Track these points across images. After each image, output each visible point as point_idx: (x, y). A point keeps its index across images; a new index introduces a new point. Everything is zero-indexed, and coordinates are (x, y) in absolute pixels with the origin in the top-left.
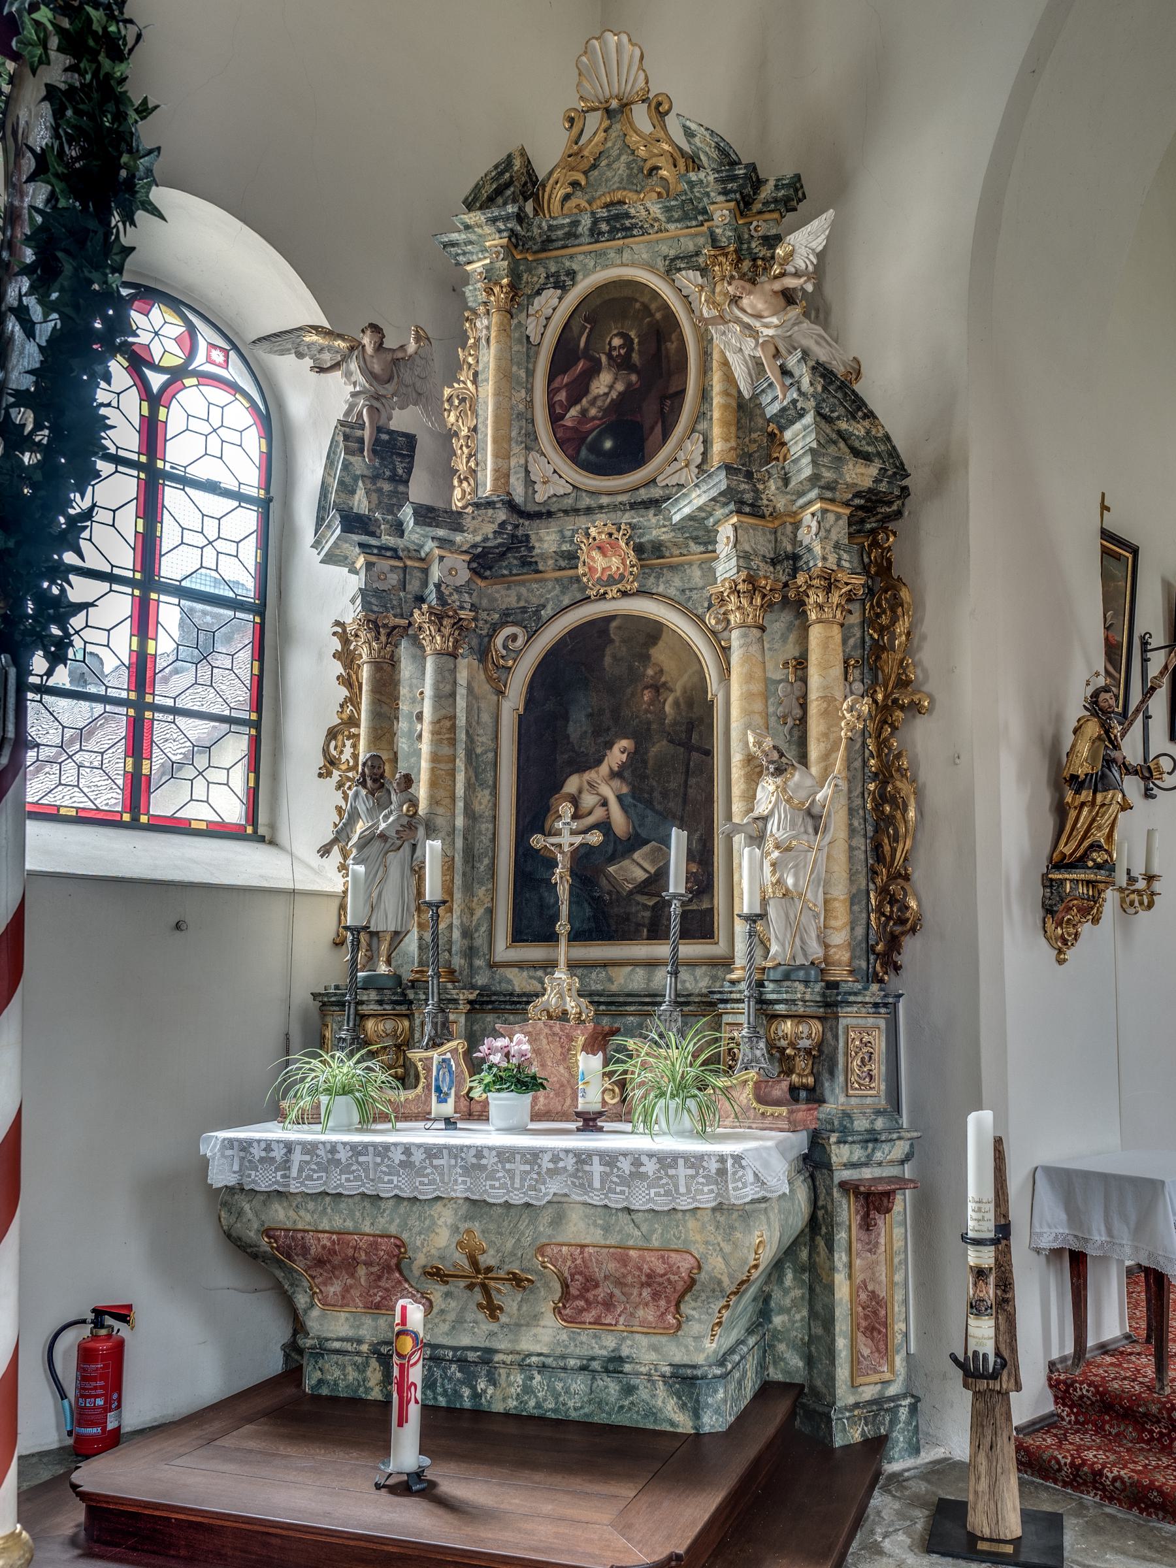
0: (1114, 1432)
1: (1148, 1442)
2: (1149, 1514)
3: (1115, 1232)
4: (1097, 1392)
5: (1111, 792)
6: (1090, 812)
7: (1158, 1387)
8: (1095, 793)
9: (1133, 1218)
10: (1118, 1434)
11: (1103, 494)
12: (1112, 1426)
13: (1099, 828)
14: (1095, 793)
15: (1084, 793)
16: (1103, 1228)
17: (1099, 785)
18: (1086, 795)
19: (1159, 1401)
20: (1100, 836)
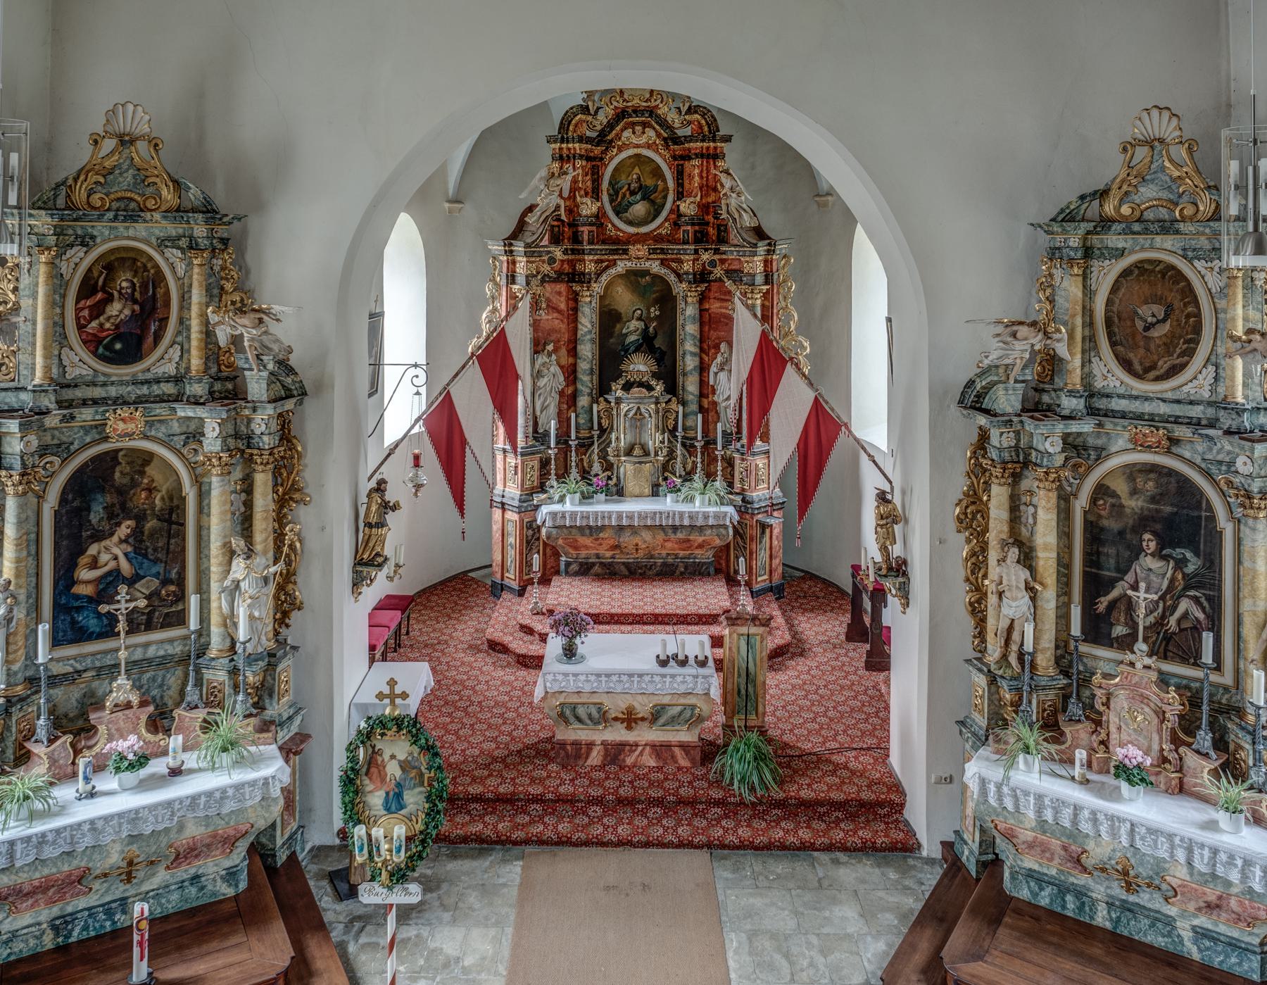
20: (378, 549)
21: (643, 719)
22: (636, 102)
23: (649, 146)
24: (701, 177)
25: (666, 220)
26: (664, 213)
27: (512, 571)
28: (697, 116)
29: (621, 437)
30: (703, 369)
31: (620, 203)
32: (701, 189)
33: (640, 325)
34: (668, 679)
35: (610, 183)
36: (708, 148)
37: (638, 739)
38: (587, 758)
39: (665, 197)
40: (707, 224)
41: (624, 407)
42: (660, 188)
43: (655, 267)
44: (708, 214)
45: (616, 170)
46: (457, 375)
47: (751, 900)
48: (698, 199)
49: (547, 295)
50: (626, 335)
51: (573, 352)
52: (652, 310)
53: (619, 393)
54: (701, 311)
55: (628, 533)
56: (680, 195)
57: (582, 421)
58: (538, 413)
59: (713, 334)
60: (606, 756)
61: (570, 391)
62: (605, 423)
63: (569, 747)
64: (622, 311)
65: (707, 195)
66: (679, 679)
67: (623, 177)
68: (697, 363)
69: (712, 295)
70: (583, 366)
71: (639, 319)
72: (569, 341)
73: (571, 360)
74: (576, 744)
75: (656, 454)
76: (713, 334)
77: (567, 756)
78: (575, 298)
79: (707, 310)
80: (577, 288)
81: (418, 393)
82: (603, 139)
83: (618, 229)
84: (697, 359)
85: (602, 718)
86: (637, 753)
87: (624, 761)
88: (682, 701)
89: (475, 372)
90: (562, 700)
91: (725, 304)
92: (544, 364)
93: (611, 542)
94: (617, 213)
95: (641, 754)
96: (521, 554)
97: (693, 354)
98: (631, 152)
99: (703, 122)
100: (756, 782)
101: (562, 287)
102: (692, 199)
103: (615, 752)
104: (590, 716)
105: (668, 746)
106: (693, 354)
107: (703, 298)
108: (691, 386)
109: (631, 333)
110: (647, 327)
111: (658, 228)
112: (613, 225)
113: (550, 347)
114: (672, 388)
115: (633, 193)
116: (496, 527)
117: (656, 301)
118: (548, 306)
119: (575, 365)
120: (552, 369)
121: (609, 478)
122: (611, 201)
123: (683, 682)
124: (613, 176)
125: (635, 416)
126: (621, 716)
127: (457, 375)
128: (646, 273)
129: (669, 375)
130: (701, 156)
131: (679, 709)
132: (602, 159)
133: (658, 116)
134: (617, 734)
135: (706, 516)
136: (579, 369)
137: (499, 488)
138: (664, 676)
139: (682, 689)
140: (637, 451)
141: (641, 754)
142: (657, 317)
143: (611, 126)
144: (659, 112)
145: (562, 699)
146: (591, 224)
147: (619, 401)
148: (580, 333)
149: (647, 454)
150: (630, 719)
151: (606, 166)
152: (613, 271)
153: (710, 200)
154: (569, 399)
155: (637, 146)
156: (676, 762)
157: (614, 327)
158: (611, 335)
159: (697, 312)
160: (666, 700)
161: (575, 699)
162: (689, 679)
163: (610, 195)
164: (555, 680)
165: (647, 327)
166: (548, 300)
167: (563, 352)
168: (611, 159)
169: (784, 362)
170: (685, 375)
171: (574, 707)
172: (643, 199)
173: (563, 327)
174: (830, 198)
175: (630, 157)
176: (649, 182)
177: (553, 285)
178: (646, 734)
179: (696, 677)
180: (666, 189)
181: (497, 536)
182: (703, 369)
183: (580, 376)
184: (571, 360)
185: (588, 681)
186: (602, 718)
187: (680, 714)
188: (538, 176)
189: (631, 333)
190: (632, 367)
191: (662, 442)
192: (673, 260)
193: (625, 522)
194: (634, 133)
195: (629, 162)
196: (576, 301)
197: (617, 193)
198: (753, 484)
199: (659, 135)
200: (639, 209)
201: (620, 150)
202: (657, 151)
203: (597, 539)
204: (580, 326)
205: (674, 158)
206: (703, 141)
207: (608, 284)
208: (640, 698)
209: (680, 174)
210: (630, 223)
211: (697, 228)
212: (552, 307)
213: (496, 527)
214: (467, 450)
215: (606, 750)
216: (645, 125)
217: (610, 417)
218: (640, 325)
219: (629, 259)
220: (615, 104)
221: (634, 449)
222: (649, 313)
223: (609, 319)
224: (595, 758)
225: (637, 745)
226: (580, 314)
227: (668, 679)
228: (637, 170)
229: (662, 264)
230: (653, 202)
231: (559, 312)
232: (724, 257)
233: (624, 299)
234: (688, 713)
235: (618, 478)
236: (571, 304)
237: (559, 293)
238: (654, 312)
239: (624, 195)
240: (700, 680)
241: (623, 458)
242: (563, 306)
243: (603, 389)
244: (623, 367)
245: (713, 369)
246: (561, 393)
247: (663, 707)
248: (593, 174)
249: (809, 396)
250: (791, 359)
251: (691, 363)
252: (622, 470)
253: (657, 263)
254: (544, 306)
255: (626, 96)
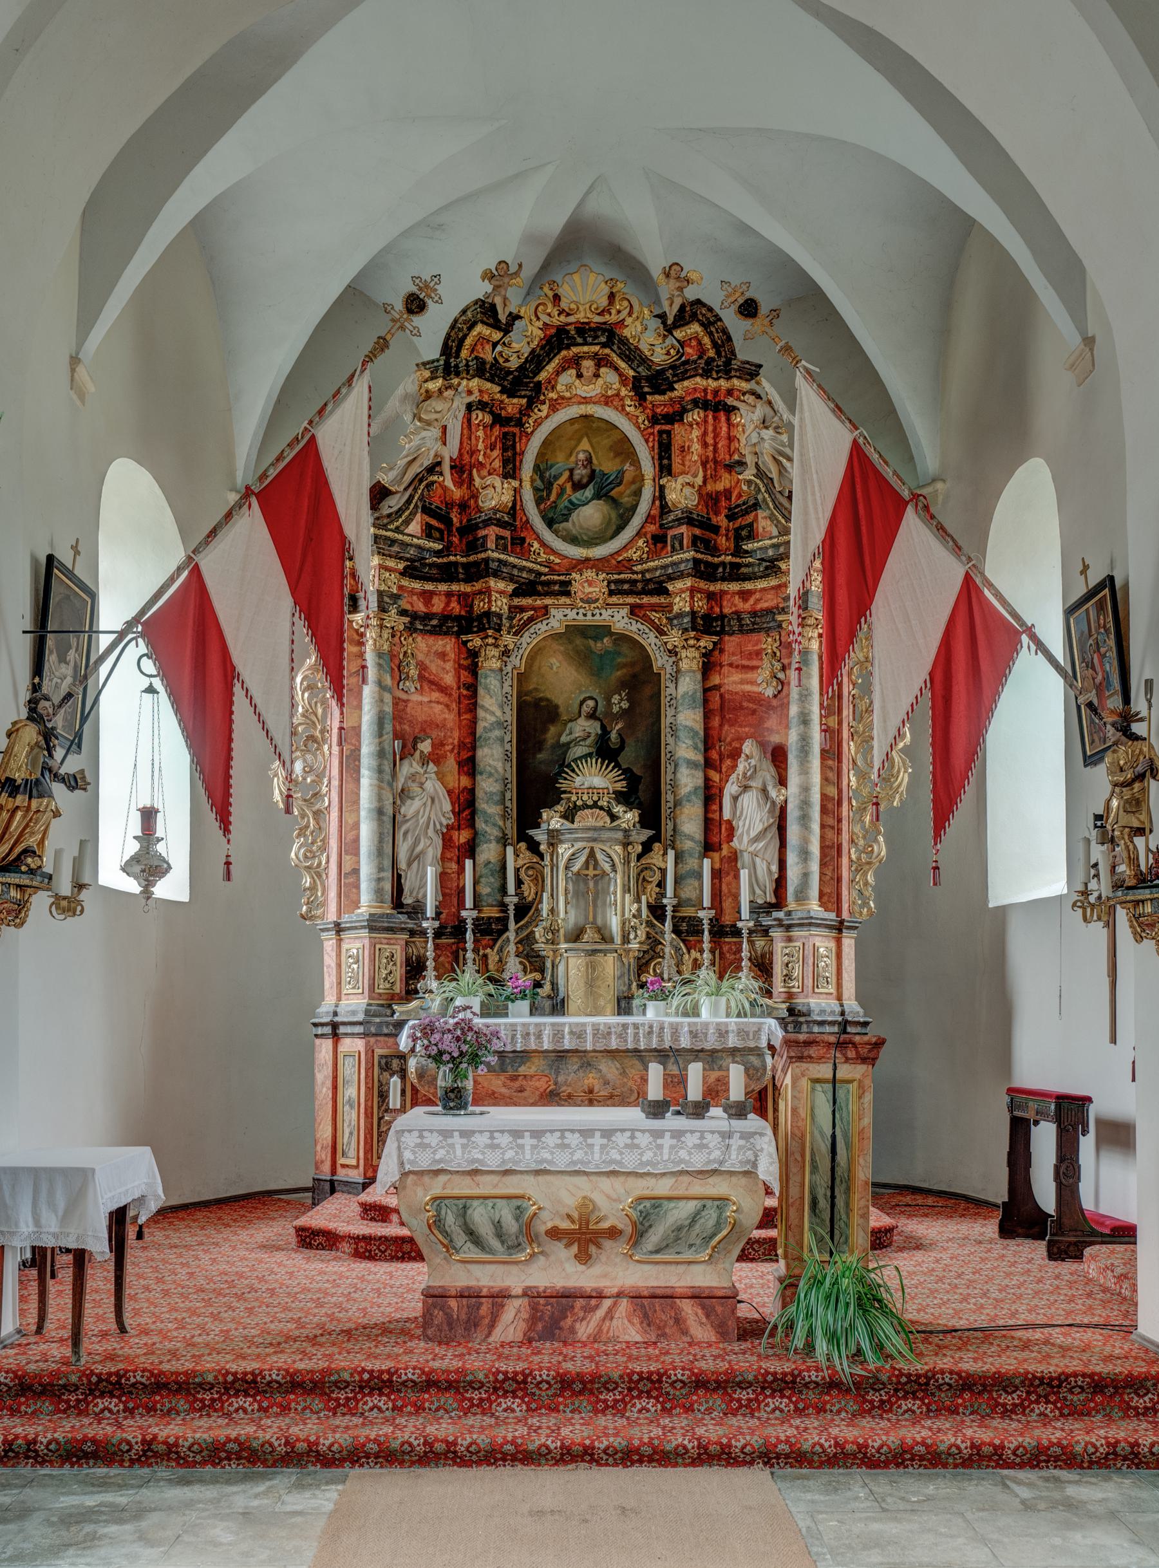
0: (29, 1411)
1: (64, 1412)
2: (81, 1466)
3: (43, 1222)
4: (16, 1376)
5: (46, 800)
6: (24, 817)
7: (73, 1360)
8: (30, 797)
9: (61, 1204)
10: (34, 1413)
11: (1114, 1040)
12: (29, 1406)
13: (32, 833)
14: (30, 797)
15: (19, 798)
16: (30, 1220)
17: (35, 792)
18: (21, 800)
19: (78, 1371)
20: (32, 841)
21: (613, 1233)
22: (581, 317)
23: (607, 401)
24: (705, 445)
25: (639, 534)
26: (636, 521)
27: (352, 1153)
28: (695, 328)
29: (560, 907)
30: (711, 796)
31: (554, 506)
32: (704, 465)
33: (594, 728)
34: (667, 1141)
35: (536, 468)
36: (716, 392)
37: (602, 1283)
38: (492, 1326)
39: (638, 493)
40: (716, 529)
41: (564, 851)
42: (628, 477)
43: (620, 620)
44: (717, 513)
45: (546, 443)
46: (213, 533)
47: (876, 1526)
48: (699, 480)
49: (420, 657)
50: (567, 746)
51: (469, 766)
52: (616, 699)
53: (556, 823)
54: (706, 691)
55: (573, 1064)
56: (665, 469)
57: (485, 890)
58: (403, 865)
59: (729, 732)
60: (533, 1320)
61: (463, 837)
62: (529, 890)
63: (453, 1303)
64: (559, 699)
65: (716, 478)
66: (691, 1140)
67: (560, 457)
68: (700, 782)
69: (726, 659)
70: (487, 786)
71: (592, 716)
72: (462, 745)
73: (465, 781)
74: (469, 1295)
75: (626, 940)
76: (729, 732)
77: (450, 1323)
78: (471, 663)
79: (717, 687)
80: (476, 641)
81: (150, 690)
82: (524, 382)
83: (553, 552)
84: (700, 775)
85: (524, 1236)
86: (600, 1313)
87: (572, 1330)
88: (699, 1188)
89: (252, 527)
90: (437, 1191)
91: (749, 676)
92: (413, 777)
93: (541, 1084)
94: (550, 523)
95: (610, 1315)
96: (369, 1115)
97: (692, 764)
98: (574, 411)
99: (706, 340)
100: (865, 1345)
101: (447, 644)
102: (688, 478)
103: (553, 1312)
104: (498, 1226)
105: (667, 1297)
106: (692, 764)
107: (708, 666)
108: (690, 822)
109: (576, 742)
110: (605, 731)
111: (625, 548)
112: (543, 544)
113: (425, 747)
114: (651, 818)
115: (578, 486)
116: (323, 1076)
117: (623, 685)
118: (421, 677)
119: (472, 791)
120: (428, 785)
121: (538, 985)
122: (539, 501)
123: (701, 1147)
124: (541, 455)
125: (587, 865)
126: (565, 1225)
127: (213, 533)
128: (604, 631)
129: (644, 794)
130: (703, 404)
131: (691, 1206)
132: (520, 424)
133: (624, 341)
134: (558, 1270)
135: (722, 1033)
136: (479, 794)
137: (330, 1000)
138: (658, 1134)
139: (698, 1161)
140: (589, 935)
141: (610, 1315)
142: (624, 713)
143: (536, 360)
144: (626, 332)
145: (438, 1187)
146: (501, 524)
147: (555, 838)
148: (481, 726)
149: (606, 938)
150: (585, 1237)
151: (529, 436)
152: (542, 628)
153: (720, 486)
154: (460, 845)
155: (586, 401)
156: (685, 1332)
157: (545, 730)
158: (540, 746)
159: (699, 687)
160: (663, 1187)
161: (464, 1187)
162: (713, 1140)
163: (536, 490)
164: (423, 1146)
165: (605, 731)
166: (422, 667)
167: (451, 764)
168: (538, 423)
169: (899, 506)
170: (677, 803)
171: (463, 1204)
172: (597, 496)
173: (450, 718)
174: (939, 486)
175: (572, 421)
176: (607, 465)
177: (431, 640)
178: (617, 1272)
179: (728, 1135)
180: (642, 478)
181: (323, 1091)
182: (711, 796)
183: (482, 805)
184: (465, 781)
185: (494, 1147)
186: (524, 1236)
187: (694, 1219)
188: (400, 391)
189: (576, 742)
190: (578, 780)
191: (637, 915)
192: (654, 608)
193: (567, 1044)
194: (579, 376)
195: (571, 429)
196: (474, 669)
197: (549, 486)
198: (809, 982)
199: (623, 379)
200: (591, 514)
201: (554, 407)
202: (622, 409)
203: (514, 1078)
204: (481, 713)
205: (654, 420)
206: (706, 374)
207: (533, 653)
208: (605, 1184)
209: (664, 451)
210: (574, 540)
211: (697, 532)
212: (427, 681)
213: (323, 1076)
214: (237, 689)
215: (534, 1308)
216: (601, 362)
217: (539, 880)
218: (594, 728)
219: (572, 606)
220: (545, 318)
221: (590, 936)
222: (609, 704)
223: (535, 717)
224: (511, 1324)
225: (601, 1296)
226: (481, 691)
227: (667, 1141)
228: (585, 445)
229: (632, 613)
230: (615, 502)
231: (443, 689)
232: (748, 586)
233: (564, 681)
234: (710, 1218)
235: (554, 985)
236: (465, 676)
237: (443, 656)
238: (619, 702)
239: (562, 489)
240: (736, 1142)
241: (564, 946)
242: (449, 679)
243: (527, 817)
244: (563, 785)
245: (731, 789)
246: (447, 841)
247: (657, 1201)
248: (504, 449)
249: (958, 573)
250: (915, 497)
251: (688, 780)
252: (561, 968)
253: (625, 611)
254: (414, 672)
255: (564, 304)
